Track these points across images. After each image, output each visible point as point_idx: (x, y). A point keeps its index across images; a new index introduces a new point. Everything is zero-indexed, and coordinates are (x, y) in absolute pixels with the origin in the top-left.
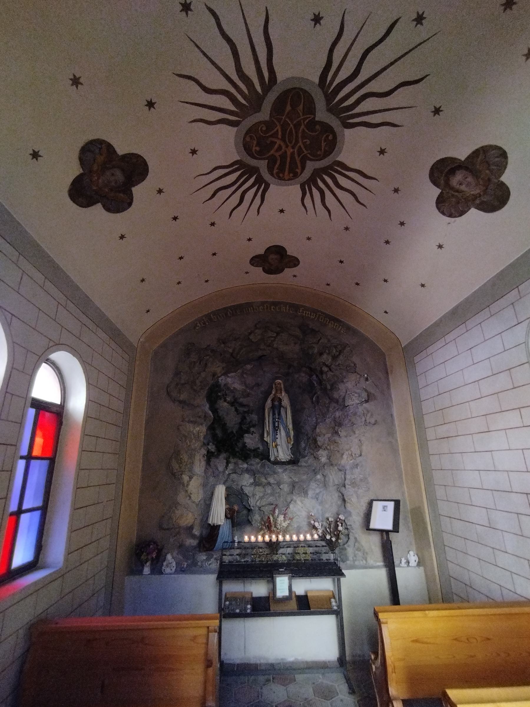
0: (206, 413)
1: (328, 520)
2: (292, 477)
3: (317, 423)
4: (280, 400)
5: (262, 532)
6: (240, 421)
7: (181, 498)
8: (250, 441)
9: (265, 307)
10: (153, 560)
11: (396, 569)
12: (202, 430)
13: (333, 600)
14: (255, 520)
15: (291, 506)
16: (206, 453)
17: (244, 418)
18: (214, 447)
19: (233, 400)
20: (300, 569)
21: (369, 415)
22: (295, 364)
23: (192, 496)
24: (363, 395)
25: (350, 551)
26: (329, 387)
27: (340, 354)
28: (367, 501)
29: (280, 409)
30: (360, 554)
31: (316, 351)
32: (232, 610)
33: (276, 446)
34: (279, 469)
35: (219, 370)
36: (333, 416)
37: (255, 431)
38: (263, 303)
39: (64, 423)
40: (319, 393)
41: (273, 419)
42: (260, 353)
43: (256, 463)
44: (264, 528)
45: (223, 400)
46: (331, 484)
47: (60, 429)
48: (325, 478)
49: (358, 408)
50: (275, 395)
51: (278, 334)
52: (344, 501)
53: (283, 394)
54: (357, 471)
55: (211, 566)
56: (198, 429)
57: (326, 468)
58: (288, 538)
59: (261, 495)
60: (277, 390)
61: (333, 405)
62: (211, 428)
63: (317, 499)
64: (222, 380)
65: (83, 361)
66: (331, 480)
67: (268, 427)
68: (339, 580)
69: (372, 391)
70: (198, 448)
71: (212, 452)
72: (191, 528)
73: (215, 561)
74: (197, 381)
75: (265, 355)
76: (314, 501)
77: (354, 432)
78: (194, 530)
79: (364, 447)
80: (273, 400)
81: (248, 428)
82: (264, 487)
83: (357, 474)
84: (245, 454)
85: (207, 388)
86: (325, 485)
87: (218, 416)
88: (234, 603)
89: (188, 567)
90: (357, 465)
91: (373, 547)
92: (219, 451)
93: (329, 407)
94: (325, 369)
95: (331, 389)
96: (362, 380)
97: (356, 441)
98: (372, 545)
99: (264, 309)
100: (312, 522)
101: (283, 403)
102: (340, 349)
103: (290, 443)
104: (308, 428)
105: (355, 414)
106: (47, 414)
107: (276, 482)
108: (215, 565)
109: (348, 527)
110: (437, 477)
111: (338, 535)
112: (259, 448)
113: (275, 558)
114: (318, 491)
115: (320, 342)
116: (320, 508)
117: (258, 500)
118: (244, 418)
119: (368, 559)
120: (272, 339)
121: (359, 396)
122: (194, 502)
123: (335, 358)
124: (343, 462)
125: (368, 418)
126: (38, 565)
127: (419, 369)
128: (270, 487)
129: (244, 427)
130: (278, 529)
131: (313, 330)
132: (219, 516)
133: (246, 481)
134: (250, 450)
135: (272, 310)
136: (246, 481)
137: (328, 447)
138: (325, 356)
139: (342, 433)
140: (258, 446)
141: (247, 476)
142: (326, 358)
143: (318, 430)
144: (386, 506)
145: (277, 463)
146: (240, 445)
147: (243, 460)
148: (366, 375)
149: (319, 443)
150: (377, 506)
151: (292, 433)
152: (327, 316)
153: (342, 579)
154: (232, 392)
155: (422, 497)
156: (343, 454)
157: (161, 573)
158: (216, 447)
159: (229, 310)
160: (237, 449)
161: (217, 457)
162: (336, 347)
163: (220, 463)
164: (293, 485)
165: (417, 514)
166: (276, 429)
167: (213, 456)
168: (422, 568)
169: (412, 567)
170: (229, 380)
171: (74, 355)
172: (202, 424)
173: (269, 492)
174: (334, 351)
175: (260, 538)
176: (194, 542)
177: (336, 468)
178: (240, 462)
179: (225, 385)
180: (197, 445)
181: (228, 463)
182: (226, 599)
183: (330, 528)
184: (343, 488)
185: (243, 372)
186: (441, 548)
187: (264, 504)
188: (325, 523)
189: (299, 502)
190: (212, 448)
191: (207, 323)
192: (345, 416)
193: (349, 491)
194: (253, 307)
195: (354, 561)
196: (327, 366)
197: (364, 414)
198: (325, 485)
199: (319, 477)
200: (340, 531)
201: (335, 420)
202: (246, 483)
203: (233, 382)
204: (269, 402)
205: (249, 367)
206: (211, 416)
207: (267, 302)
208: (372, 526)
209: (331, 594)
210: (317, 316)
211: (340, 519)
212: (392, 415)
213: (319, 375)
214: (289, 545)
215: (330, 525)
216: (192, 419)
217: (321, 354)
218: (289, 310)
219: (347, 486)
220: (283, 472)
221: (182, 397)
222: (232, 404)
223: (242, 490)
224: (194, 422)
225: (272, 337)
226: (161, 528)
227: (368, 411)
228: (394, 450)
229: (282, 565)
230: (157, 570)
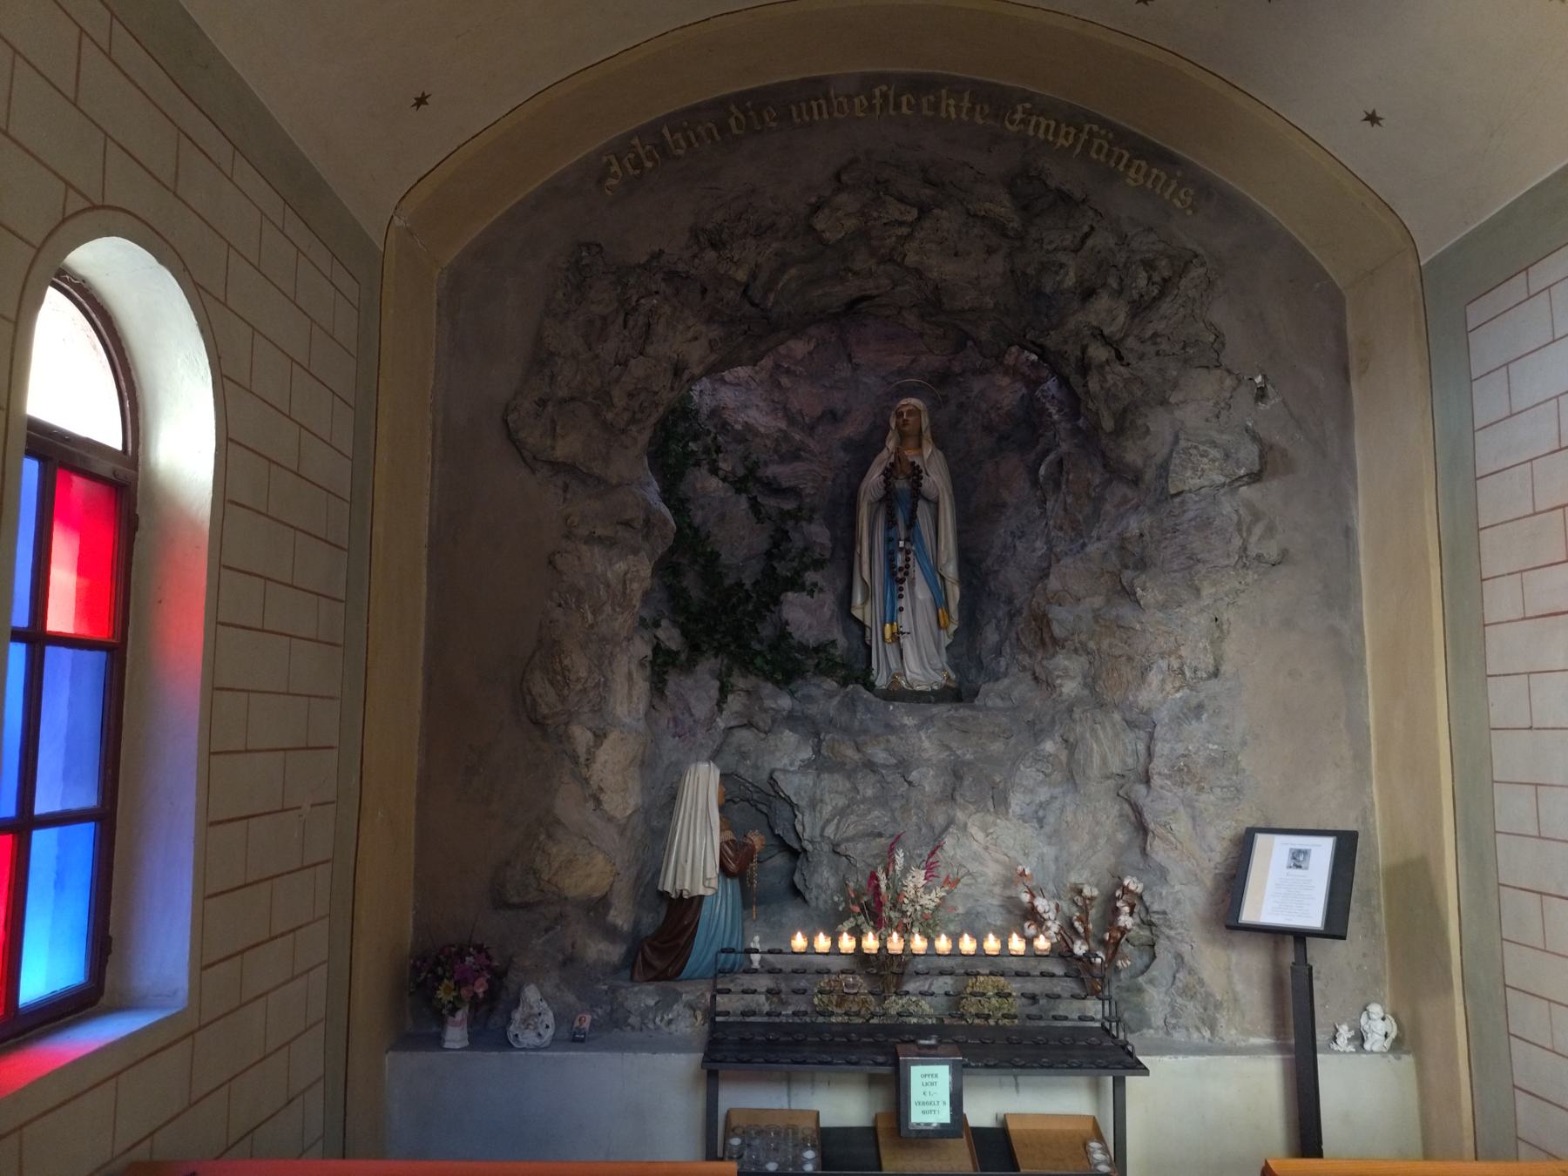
0: (648, 509)
1: (1080, 892)
2: (954, 745)
3: (1051, 558)
4: (916, 474)
5: (848, 924)
6: (765, 546)
7: (568, 805)
8: (805, 616)
9: (877, 101)
10: (475, 1003)
11: (1319, 1056)
12: (633, 570)
13: (1094, 1145)
14: (819, 887)
15: (948, 842)
16: (649, 653)
17: (780, 538)
18: (676, 632)
19: (741, 472)
20: (989, 1047)
21: (1258, 530)
22: (984, 334)
23: (604, 797)
24: (1242, 454)
25: (1156, 999)
26: (1108, 424)
27: (1162, 294)
28: (1228, 834)
29: (915, 506)
30: (1193, 1008)
31: (1070, 281)
32: (756, 1163)
33: (896, 637)
34: (906, 718)
35: (696, 354)
36: (1114, 533)
37: (822, 583)
38: (869, 82)
39: (143, 522)
40: (1064, 447)
41: (889, 540)
42: (852, 288)
43: (823, 696)
44: (857, 909)
45: (704, 470)
46: (1095, 770)
47: (130, 541)
48: (1071, 754)
49: (1215, 501)
50: (898, 453)
51: (924, 211)
52: (1142, 829)
53: (928, 450)
54: (1197, 728)
55: (673, 1027)
56: (620, 567)
57: (1076, 716)
58: (943, 944)
59: (841, 802)
60: (903, 436)
61: (1120, 490)
62: (667, 568)
63: (1041, 821)
64: (704, 395)
65: (196, 284)
66: (1096, 760)
67: (869, 565)
68: (1119, 1084)
69: (1278, 439)
70: (624, 633)
71: (669, 652)
72: (598, 906)
73: (689, 1012)
74: (618, 395)
75: (870, 298)
76: (1029, 830)
77: (1197, 591)
78: (612, 912)
79: (1230, 648)
80: (889, 473)
81: (798, 573)
82: (849, 776)
83: (1197, 740)
84: (786, 663)
85: (653, 420)
86: (1072, 776)
87: (690, 526)
88: (757, 1142)
89: (599, 1026)
90: (1200, 707)
91: (1239, 987)
92: (695, 649)
93: (1100, 499)
94: (1099, 353)
95: (1119, 431)
96: (1245, 397)
97: (1204, 620)
98: (1239, 976)
99: (871, 107)
100: (1026, 898)
101: (926, 485)
102: (1166, 274)
103: (946, 628)
104: (1012, 577)
105: (1205, 524)
106: (79, 484)
107: (894, 761)
108: (687, 1025)
109: (1155, 918)
110: (1510, 756)
111: (1117, 943)
112: (833, 643)
113: (895, 1005)
114: (1043, 794)
115: (1090, 243)
116: (1049, 851)
117: (828, 821)
118: (780, 538)
119: (1222, 1021)
120: (904, 231)
121: (1227, 456)
122: (610, 819)
123: (1140, 308)
124: (1145, 697)
125: (1253, 539)
126: (103, 1001)
127: (1486, 348)
128: (872, 778)
129: (783, 569)
130: (904, 913)
131: (1064, 197)
132: (699, 865)
133: (787, 756)
134: (803, 648)
135: (904, 109)
136: (787, 756)
137: (1092, 645)
138: (1103, 302)
139: (1150, 594)
140: (831, 637)
141: (789, 737)
142: (1107, 312)
143: (1054, 583)
144: (1306, 853)
145: (898, 694)
146: (766, 631)
147: (776, 683)
148: (1259, 379)
149: (1058, 630)
150: (1272, 852)
151: (955, 593)
152: (1121, 137)
153: (1133, 1082)
154: (740, 438)
155: (1441, 827)
156: (1145, 670)
157: (504, 1043)
158: (685, 633)
159: (733, 108)
160: (756, 646)
161: (688, 668)
162: (1149, 265)
163: (697, 689)
164: (956, 773)
165: (1414, 883)
166: (896, 578)
167: (674, 666)
168: (1408, 1060)
169: (1372, 1052)
170: (727, 396)
171: (161, 261)
172: (635, 551)
173: (869, 793)
174: (1142, 281)
175: (1017, 944)
176: (614, 952)
177: (1117, 717)
178: (768, 688)
179: (714, 413)
180: (621, 623)
181: (724, 691)
182: (730, 1131)
183: (1084, 922)
184: (1141, 789)
185: (777, 366)
186: (1492, 998)
187: (851, 832)
188: (1064, 905)
189: (974, 830)
190: (670, 636)
191: (649, 164)
192: (1164, 531)
193: (1164, 802)
194: (828, 99)
195: (1168, 1028)
196: (1106, 341)
197: (1239, 523)
198: (1072, 776)
199: (1049, 746)
200: (1124, 931)
201: (1122, 546)
202: (786, 761)
203: (741, 400)
204: (875, 476)
205: (799, 347)
206: (666, 522)
207: (882, 78)
208: (1248, 916)
209: (1089, 1127)
210: (1084, 136)
211: (1126, 890)
212: (1348, 533)
213: (1075, 379)
214: (934, 965)
215: (1084, 910)
216: (599, 532)
217: (1088, 294)
218: (971, 110)
219: (1156, 781)
220: (919, 727)
221: (562, 451)
222: (739, 485)
223: (772, 781)
224: (609, 543)
225: (901, 223)
226: (500, 903)
227: (1257, 516)
228: (1348, 662)
229: (923, 1031)
230: (491, 1030)
